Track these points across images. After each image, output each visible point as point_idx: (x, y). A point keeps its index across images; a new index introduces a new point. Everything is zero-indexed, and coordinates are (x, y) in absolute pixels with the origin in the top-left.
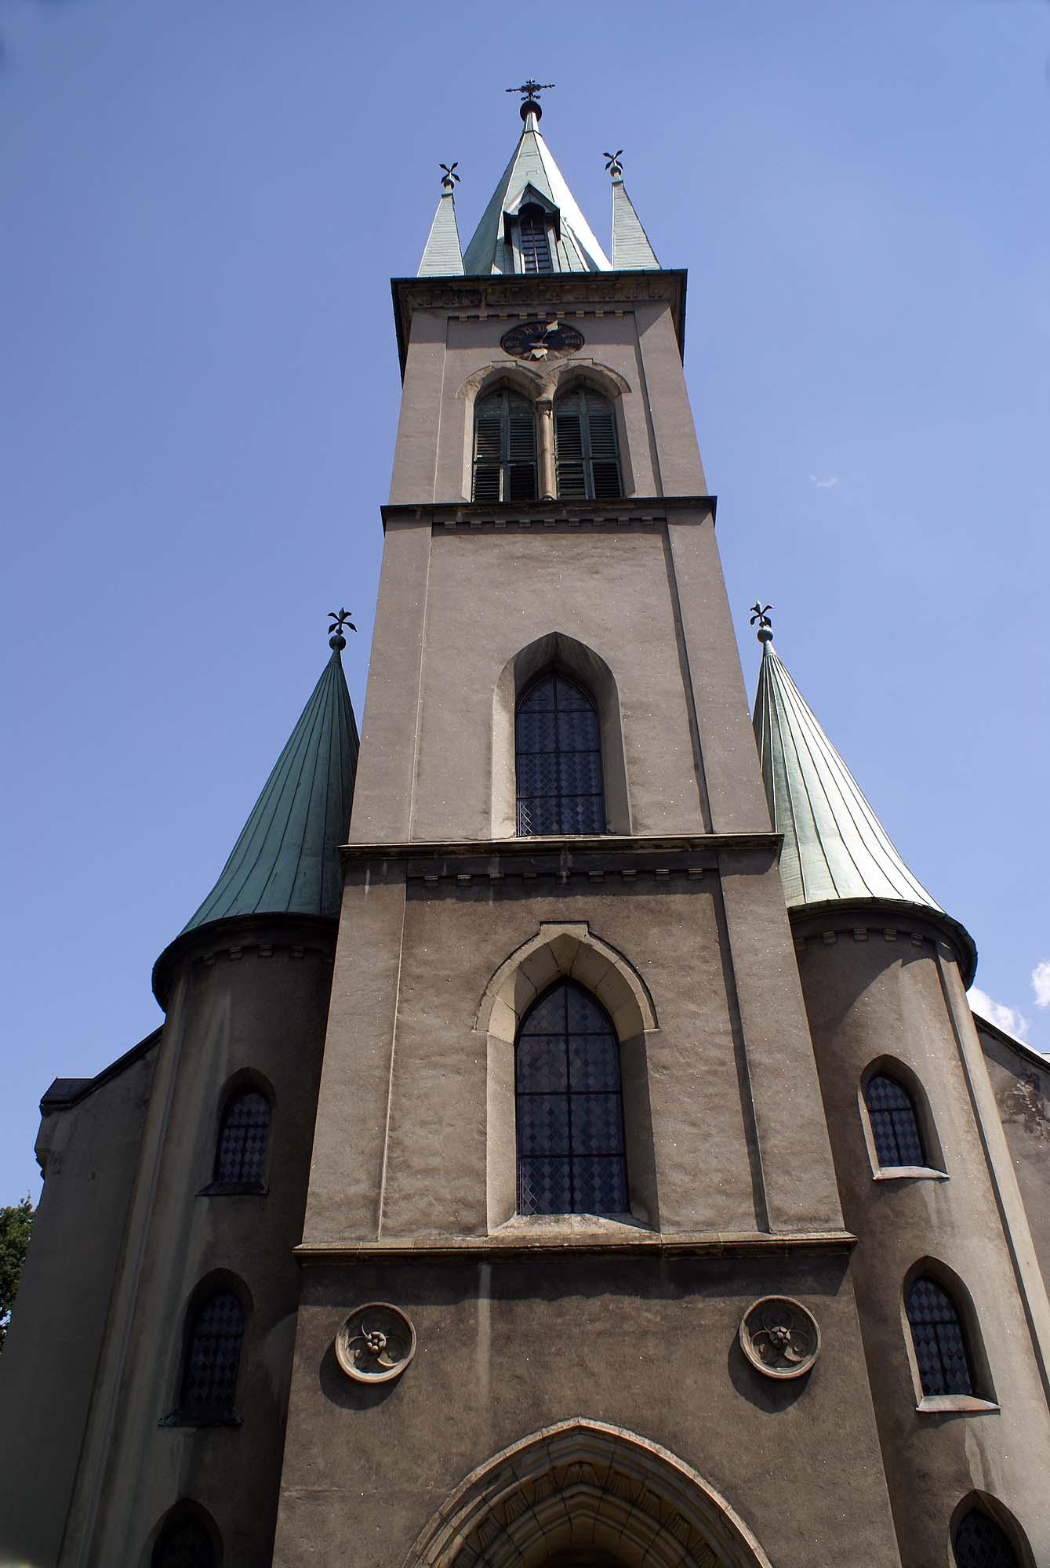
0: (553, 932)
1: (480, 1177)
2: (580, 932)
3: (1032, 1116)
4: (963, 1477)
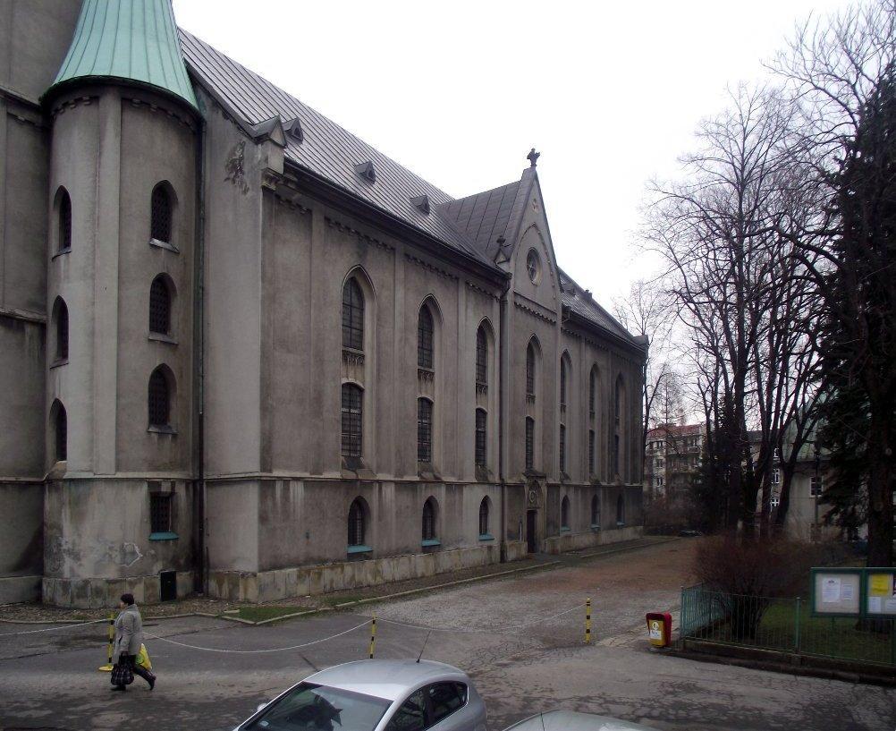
4: (54, 394)
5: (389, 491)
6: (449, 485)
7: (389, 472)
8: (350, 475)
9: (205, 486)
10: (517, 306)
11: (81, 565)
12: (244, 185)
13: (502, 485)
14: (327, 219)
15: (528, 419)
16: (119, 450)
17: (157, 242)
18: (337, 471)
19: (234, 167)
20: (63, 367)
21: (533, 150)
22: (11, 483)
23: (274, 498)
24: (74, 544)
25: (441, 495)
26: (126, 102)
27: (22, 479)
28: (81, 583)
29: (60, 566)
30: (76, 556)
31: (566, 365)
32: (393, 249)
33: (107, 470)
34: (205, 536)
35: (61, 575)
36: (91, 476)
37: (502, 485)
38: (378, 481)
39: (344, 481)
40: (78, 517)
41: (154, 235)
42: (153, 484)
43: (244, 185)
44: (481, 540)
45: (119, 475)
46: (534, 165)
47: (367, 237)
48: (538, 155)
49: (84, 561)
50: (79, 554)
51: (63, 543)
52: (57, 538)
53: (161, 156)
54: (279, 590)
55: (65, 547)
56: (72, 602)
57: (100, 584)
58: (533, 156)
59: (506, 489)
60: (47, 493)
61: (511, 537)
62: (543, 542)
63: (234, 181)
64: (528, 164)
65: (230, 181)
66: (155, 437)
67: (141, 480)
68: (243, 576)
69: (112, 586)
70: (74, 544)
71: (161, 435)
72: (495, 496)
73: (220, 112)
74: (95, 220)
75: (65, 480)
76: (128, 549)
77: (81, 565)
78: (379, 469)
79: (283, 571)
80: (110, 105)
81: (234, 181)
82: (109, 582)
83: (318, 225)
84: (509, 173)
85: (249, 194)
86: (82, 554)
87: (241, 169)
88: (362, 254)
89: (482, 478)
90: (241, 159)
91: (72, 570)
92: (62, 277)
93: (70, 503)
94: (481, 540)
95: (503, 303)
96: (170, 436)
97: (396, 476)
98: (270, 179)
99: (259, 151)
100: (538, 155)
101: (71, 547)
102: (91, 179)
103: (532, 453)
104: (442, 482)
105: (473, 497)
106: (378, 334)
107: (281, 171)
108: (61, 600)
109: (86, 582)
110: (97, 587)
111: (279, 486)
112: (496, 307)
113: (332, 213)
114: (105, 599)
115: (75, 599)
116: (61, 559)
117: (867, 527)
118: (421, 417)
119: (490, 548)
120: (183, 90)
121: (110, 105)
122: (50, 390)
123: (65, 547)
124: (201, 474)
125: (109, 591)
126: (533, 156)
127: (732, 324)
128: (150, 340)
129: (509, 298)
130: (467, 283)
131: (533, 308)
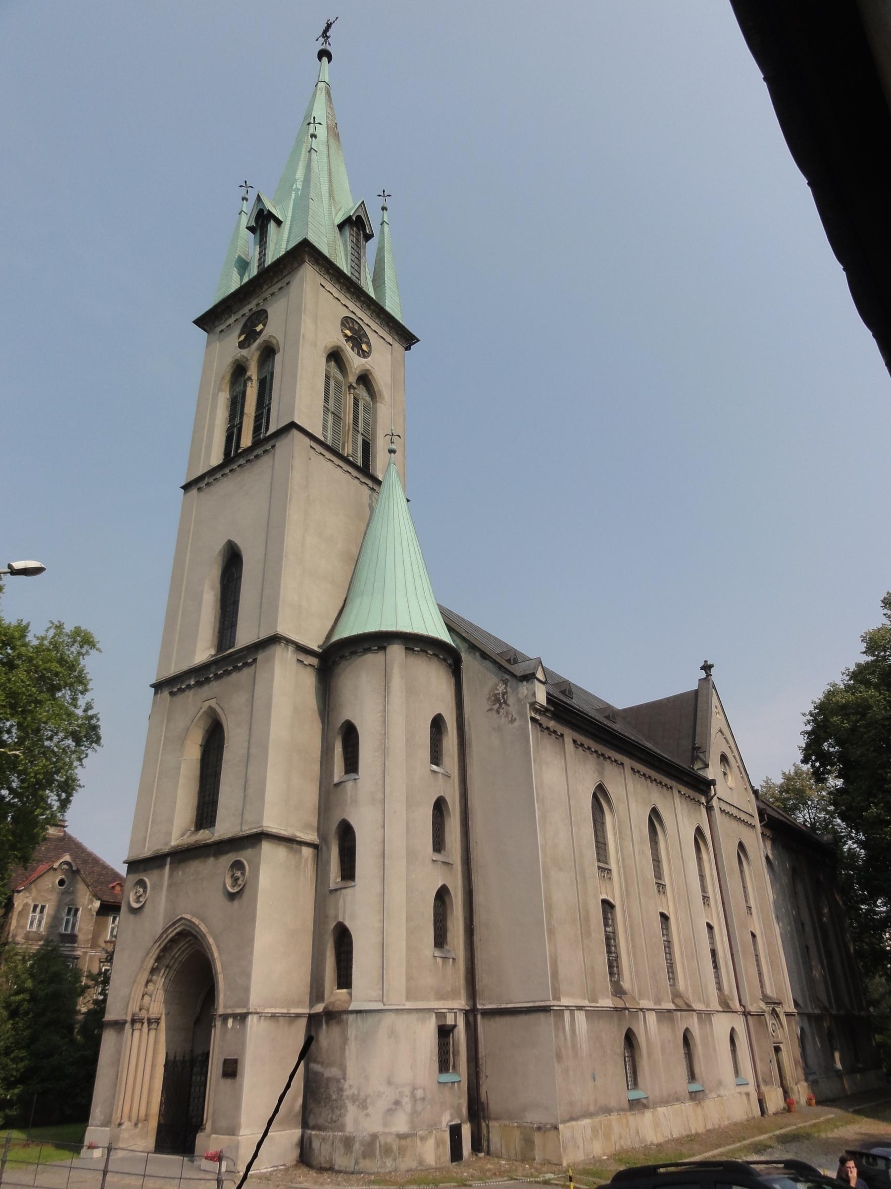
0: (207, 704)
1: (171, 821)
2: (213, 703)
3: (501, 704)
4: (336, 916)
5: (652, 1018)
6: (700, 1013)
7: (649, 999)
8: (621, 1004)
9: (479, 1017)
10: (723, 811)
11: (367, 1115)
12: (510, 716)
13: (746, 1014)
14: (575, 742)
15: (605, 902)
16: (409, 978)
17: (434, 767)
18: (608, 997)
19: (497, 700)
20: (349, 890)
22: (284, 1015)
23: (564, 1029)
25: (693, 1024)
27: (294, 1011)
28: (368, 1138)
29: (340, 1115)
30: (363, 1106)
31: (744, 863)
32: (622, 764)
33: (397, 1000)
34: (484, 1078)
35: (342, 1128)
36: (380, 1006)
37: (746, 1014)
38: (641, 1009)
39: (616, 1009)
41: (432, 763)
42: (440, 1015)
43: (510, 716)
44: (180, 1126)
45: (409, 1005)
46: (708, 675)
47: (603, 755)
48: (711, 666)
49: (370, 1110)
50: (365, 1101)
51: (346, 1086)
52: (338, 1081)
53: (433, 687)
54: (578, 1147)
55: (348, 1093)
56: (356, 1163)
57: (389, 1140)
58: (707, 668)
59: (749, 1017)
60: (324, 1026)
61: (766, 1083)
62: (795, 1088)
63: (498, 712)
64: (703, 674)
65: (494, 712)
66: (439, 960)
67: (430, 1010)
68: (539, 1129)
69: (403, 1142)
71: (444, 958)
72: (739, 1024)
73: (478, 654)
74: (384, 751)
75: (352, 1012)
77: (367, 1115)
78: (641, 996)
79: (579, 1122)
80: (396, 651)
81: (498, 712)
82: (401, 1137)
83: (569, 746)
85: (516, 724)
87: (505, 702)
88: (601, 772)
89: (727, 1008)
90: (504, 694)
91: (356, 1121)
92: (349, 801)
94: (180, 1126)
95: (709, 809)
96: (451, 960)
97: (655, 1004)
98: (536, 711)
99: (524, 689)
100: (711, 666)
101: (356, 1092)
102: (379, 715)
103: (617, 958)
104: (694, 1010)
105: (722, 1025)
106: (621, 848)
107: (545, 704)
108: (341, 1161)
109: (374, 1137)
110: (386, 1144)
111: (567, 1014)
112: (704, 810)
113: (581, 739)
114: (395, 1160)
115: (361, 1160)
116: (344, 1106)
118: (606, 925)
119: (748, 1094)
120: (445, 636)
121: (396, 651)
122: (331, 912)
124: (474, 1004)
125: (399, 1148)
126: (707, 668)
128: (434, 861)
129: (715, 802)
130: (679, 792)
131: (735, 812)
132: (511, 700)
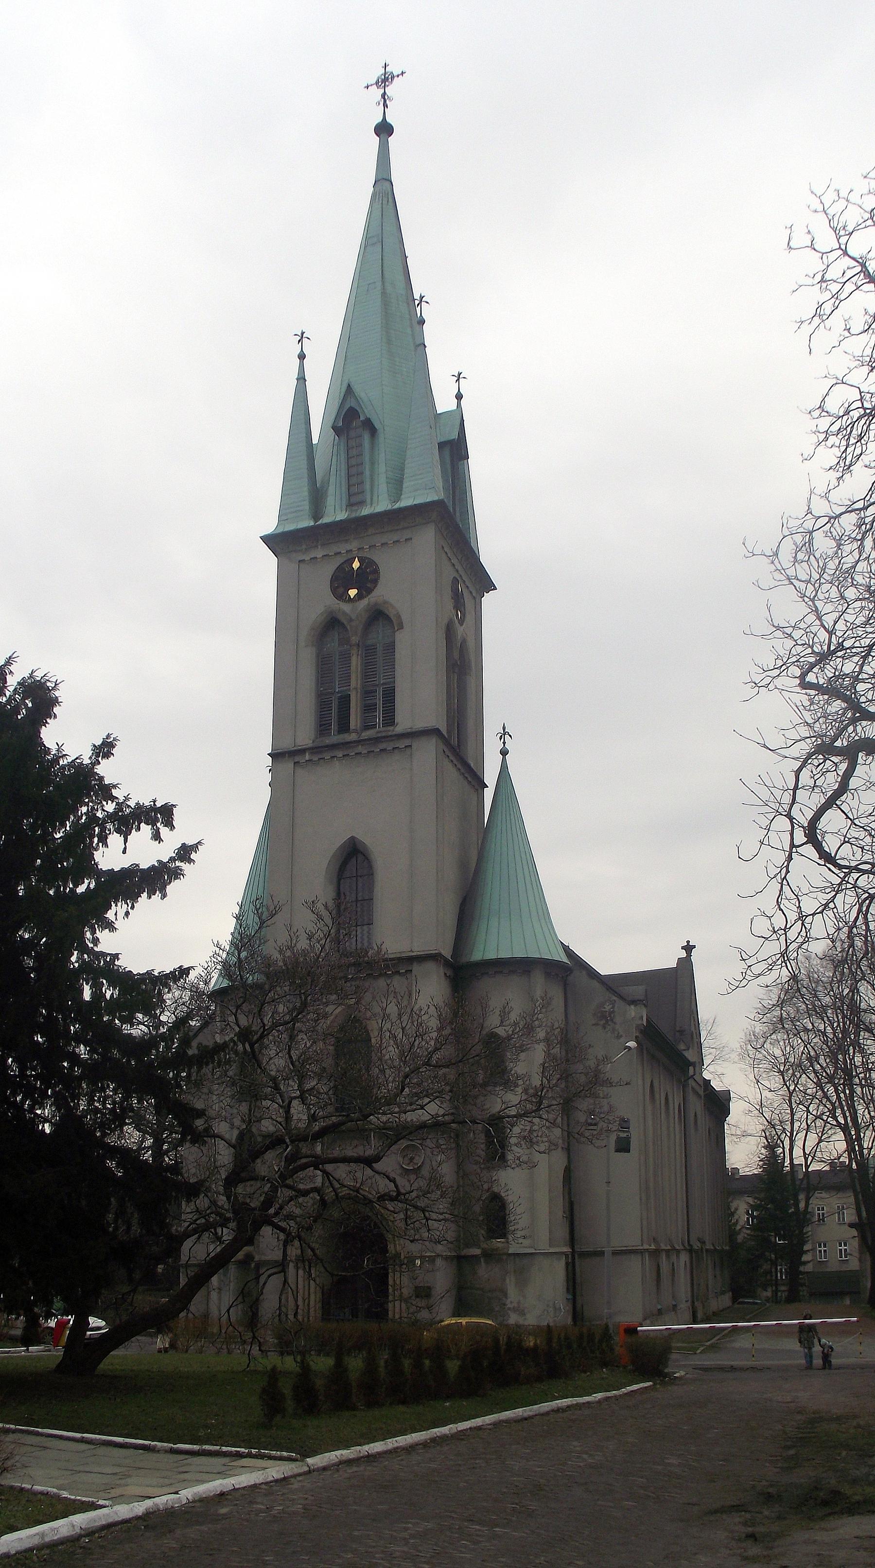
3: (607, 1021)
21: (688, 942)
24: (519, 1303)
26: (548, 975)
40: (522, 1282)
46: (689, 954)
63: (604, 1028)
64: (683, 954)
70: (519, 1303)
73: (584, 973)
76: (557, 1307)
81: (604, 1028)
84: (668, 960)
86: (526, 1311)
87: (612, 1020)
90: (611, 1013)
93: (515, 1271)
101: (516, 1305)
117: (101, 1366)
120: (565, 960)
123: (509, 1306)
127: (366, 940)
132: (618, 1019)
